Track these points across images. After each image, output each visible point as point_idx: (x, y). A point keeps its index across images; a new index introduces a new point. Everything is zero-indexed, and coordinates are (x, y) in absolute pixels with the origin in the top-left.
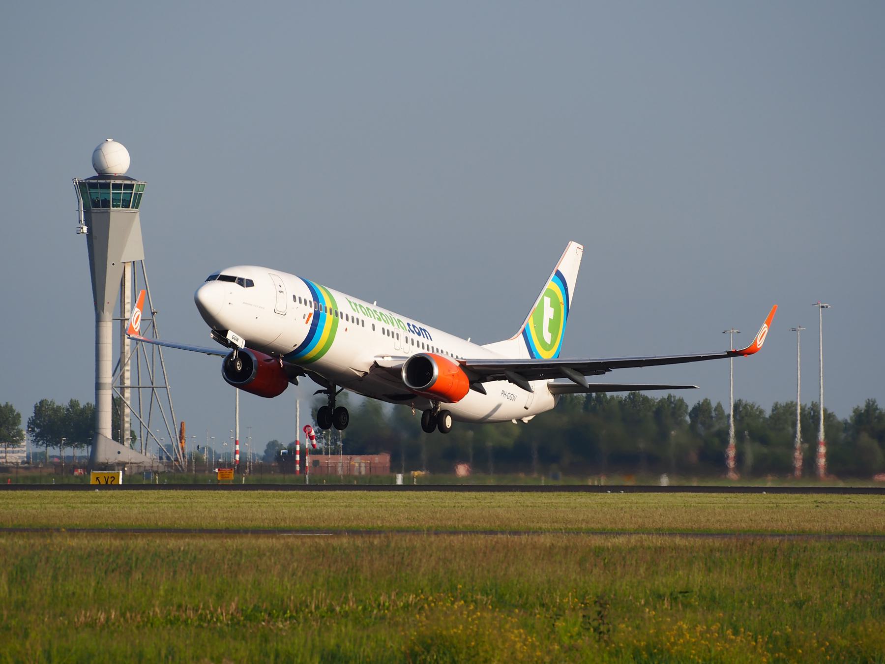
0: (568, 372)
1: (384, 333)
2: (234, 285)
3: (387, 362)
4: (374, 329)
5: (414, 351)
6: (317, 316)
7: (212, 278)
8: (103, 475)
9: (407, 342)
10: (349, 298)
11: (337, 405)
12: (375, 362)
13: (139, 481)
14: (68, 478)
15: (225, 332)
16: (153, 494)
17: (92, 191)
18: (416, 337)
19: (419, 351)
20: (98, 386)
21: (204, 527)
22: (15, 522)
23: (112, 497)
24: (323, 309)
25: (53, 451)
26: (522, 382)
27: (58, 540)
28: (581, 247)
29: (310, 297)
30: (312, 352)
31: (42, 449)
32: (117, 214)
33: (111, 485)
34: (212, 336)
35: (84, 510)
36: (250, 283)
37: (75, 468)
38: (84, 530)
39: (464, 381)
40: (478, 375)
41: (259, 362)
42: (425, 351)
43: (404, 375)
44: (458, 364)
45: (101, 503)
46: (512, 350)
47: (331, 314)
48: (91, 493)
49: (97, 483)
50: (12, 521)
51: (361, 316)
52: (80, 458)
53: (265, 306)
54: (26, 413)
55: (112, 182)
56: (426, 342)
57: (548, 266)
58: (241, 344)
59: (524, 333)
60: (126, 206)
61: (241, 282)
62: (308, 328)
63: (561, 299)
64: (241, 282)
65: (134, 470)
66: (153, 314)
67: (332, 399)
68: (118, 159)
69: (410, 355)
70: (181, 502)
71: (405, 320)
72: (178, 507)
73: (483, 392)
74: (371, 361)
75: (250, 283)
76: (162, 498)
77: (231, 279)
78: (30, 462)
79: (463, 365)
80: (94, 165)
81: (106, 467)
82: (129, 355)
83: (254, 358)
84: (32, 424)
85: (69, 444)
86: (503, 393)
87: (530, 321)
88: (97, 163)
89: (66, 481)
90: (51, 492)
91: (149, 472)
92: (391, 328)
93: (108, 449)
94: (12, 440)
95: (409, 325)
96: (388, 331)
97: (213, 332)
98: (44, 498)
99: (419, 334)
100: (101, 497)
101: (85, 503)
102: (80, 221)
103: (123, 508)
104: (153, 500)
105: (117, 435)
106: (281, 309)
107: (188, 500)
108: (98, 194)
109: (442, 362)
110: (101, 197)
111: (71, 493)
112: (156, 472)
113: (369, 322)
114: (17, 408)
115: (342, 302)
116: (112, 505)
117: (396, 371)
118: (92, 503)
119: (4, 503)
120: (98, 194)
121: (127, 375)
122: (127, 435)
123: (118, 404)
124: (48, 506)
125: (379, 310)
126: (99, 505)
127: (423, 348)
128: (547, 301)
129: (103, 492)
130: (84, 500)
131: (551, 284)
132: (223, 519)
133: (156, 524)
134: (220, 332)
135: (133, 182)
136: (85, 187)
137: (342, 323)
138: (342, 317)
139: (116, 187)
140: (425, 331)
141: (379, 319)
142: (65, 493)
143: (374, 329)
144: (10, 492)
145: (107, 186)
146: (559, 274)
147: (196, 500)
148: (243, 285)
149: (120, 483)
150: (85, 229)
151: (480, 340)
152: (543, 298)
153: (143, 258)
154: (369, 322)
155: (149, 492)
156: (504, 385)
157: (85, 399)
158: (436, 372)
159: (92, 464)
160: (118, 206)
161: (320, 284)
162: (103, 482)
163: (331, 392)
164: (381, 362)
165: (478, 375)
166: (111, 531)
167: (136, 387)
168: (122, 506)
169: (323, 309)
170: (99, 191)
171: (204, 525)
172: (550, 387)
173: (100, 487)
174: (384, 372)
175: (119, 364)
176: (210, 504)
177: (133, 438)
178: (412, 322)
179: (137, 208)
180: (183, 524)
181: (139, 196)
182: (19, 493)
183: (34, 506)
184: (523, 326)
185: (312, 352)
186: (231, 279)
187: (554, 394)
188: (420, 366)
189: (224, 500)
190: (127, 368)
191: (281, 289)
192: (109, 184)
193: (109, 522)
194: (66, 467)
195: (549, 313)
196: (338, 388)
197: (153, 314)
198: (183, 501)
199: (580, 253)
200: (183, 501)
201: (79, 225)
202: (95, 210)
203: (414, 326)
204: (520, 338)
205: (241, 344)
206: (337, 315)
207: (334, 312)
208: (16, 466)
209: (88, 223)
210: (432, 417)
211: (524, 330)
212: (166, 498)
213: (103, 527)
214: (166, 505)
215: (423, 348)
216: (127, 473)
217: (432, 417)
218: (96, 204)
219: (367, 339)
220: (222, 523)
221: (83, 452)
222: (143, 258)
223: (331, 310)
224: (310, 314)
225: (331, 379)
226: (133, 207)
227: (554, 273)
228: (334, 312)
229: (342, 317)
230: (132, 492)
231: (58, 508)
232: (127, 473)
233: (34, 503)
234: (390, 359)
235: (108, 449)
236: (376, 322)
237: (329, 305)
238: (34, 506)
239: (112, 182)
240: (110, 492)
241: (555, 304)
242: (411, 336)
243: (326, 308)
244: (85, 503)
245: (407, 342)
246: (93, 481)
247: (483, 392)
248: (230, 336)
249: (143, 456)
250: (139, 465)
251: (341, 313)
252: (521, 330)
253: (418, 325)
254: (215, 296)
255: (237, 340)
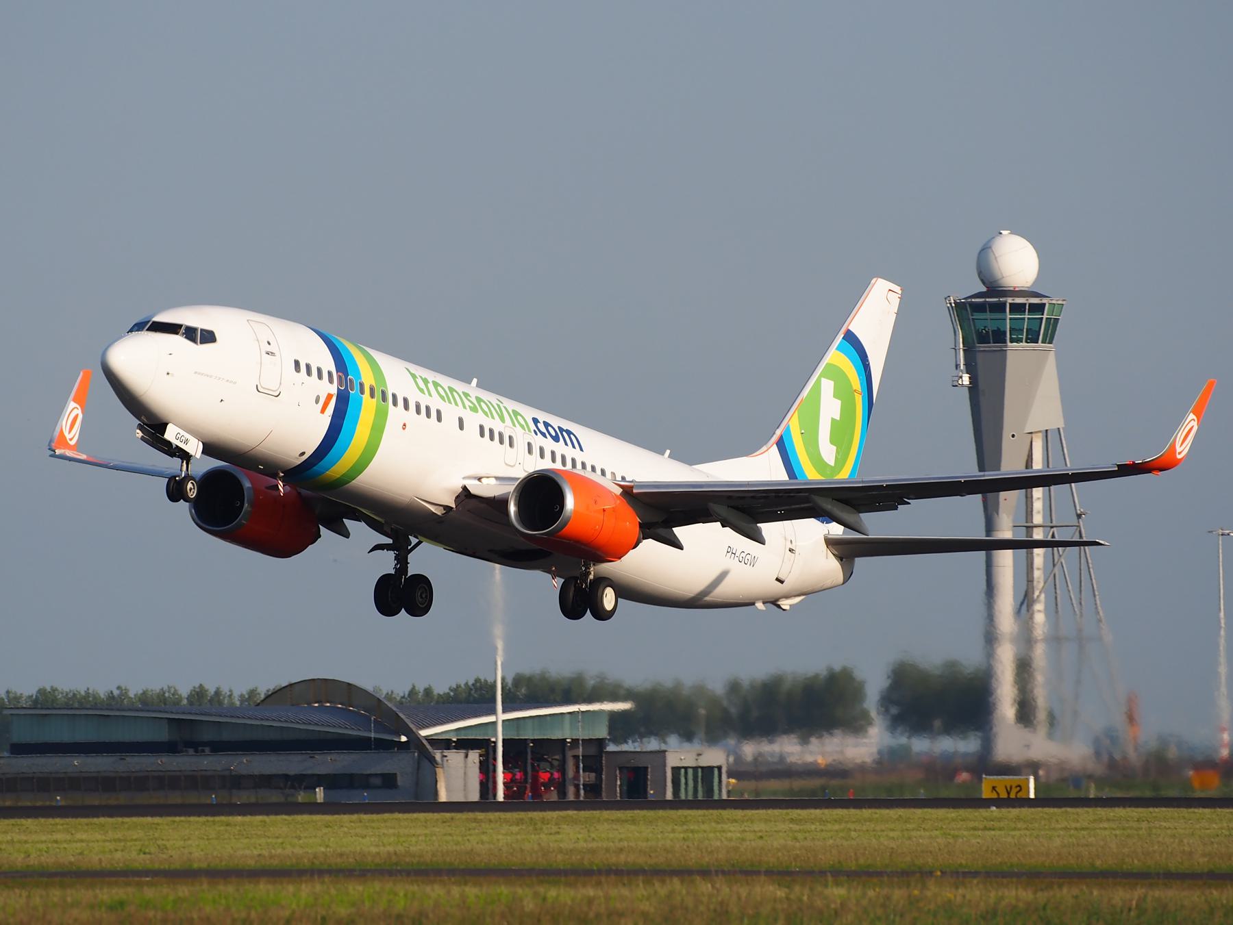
0: (828, 505)
1: (482, 435)
2: (178, 340)
3: (488, 488)
4: (461, 427)
5: (526, 465)
6: (343, 401)
7: (139, 327)
8: (1002, 781)
9: (530, 451)
10: (415, 369)
11: (412, 571)
12: (465, 488)
13: (1062, 793)
14: (946, 789)
15: (163, 427)
16: (1085, 815)
17: (977, 316)
18: (549, 444)
19: (546, 464)
20: (991, 638)
21: (1173, 869)
22: (862, 861)
23: (1018, 819)
24: (357, 387)
25: (921, 745)
26: (743, 524)
27: (932, 889)
28: (897, 289)
29: (329, 364)
30: (339, 466)
31: (903, 740)
32: (1018, 354)
33: (1017, 799)
34: (139, 434)
35: (973, 841)
36: (208, 337)
37: (955, 771)
38: (975, 874)
39: (630, 521)
40: (664, 512)
41: (255, 489)
42: (558, 465)
43: (512, 508)
44: (619, 491)
45: (1000, 829)
46: (761, 469)
47: (372, 396)
48: (983, 812)
49: (994, 796)
50: (857, 860)
51: (435, 403)
52: (966, 755)
53: (244, 381)
54: (875, 683)
55: (1010, 300)
56: (570, 453)
57: (830, 320)
58: (194, 447)
59: (781, 445)
60: (1035, 340)
61: (190, 333)
62: (325, 421)
63: (856, 382)
64: (190, 333)
65: (1054, 776)
66: (1079, 516)
67: (402, 562)
68: (1018, 263)
69: (522, 474)
70: (1131, 828)
71: (528, 413)
72: (1128, 836)
73: (677, 545)
74: (456, 484)
75: (208, 337)
76: (1101, 820)
77: (172, 329)
78: (890, 760)
79: (628, 492)
80: (980, 274)
81: (1006, 769)
82: (1042, 584)
83: (247, 484)
84: (887, 700)
85: (948, 730)
86: (730, 551)
87: (793, 424)
88: (985, 272)
89: (945, 793)
90: (919, 812)
91: (1076, 779)
92: (498, 427)
93: (1010, 741)
94: (855, 724)
95: (535, 421)
96: (491, 431)
97: (140, 427)
98: (907, 821)
99: (556, 439)
100: (1000, 819)
101: (975, 829)
102: (957, 366)
103: (1037, 837)
104: (1085, 824)
105: (1025, 713)
106: (270, 384)
107: (1144, 825)
108: (986, 321)
109: (584, 486)
110: (991, 326)
111: (951, 813)
112: (1090, 777)
113: (452, 414)
114: (859, 674)
115: (397, 375)
116: (1017, 833)
117: (499, 504)
118: (985, 829)
119: (843, 830)
120: (986, 321)
121: (1040, 618)
122: (1041, 715)
123: (1024, 667)
124: (914, 833)
125: (487, 396)
126: (998, 833)
127: (554, 460)
128: (827, 386)
129: (1004, 810)
130: (972, 824)
131: (837, 357)
132: (1204, 855)
133: (1093, 865)
134: (154, 428)
135: (1044, 301)
136: (964, 311)
137: (396, 414)
138: (395, 403)
139: (1017, 308)
140: (569, 433)
141: (474, 409)
142: (941, 812)
143: (461, 427)
144: (853, 811)
145: (1000, 308)
146: (851, 338)
147: (1157, 824)
148: (193, 340)
149: (1032, 796)
150: (966, 379)
151: (689, 458)
152: (819, 380)
153: (1061, 425)
154: (452, 414)
155: (1079, 810)
156: (713, 530)
157: (969, 657)
158: (570, 503)
159: (984, 765)
160: (1019, 341)
161: (356, 342)
162: (1004, 795)
163: (402, 550)
164: (476, 488)
165: (664, 512)
166: (1018, 875)
167: (1055, 639)
168: (1035, 833)
169: (357, 387)
170: (988, 315)
171: (1173, 866)
172: (831, 543)
173: (999, 803)
174: (483, 505)
175: (1025, 602)
176: (1182, 831)
177: (1052, 719)
178: (543, 417)
179: (1050, 343)
180: (1136, 864)
181: (1053, 324)
182: (866, 813)
183: (892, 834)
184: (778, 432)
185: (339, 466)
186: (172, 329)
187: (840, 558)
188: (541, 492)
189: (1204, 824)
190: (1039, 607)
191: (269, 348)
192: (1004, 304)
193: (1015, 860)
194: (941, 770)
195: (830, 408)
196: (414, 541)
197: (1079, 516)
198: (1135, 825)
199: (895, 300)
200: (1135, 825)
201: (955, 373)
202: (982, 347)
203: (546, 425)
204: (774, 450)
205: (194, 447)
206: (384, 399)
207: (378, 394)
208: (862, 768)
209: (970, 368)
210: (578, 590)
211: (781, 438)
212: (1108, 820)
213: (1005, 868)
214: (1107, 833)
215: (554, 460)
216: (1043, 780)
217: (578, 590)
218: (983, 338)
219: (443, 441)
220: (1201, 862)
221: (964, 745)
222: (1061, 425)
223: (372, 390)
224: (330, 396)
225: (400, 523)
226: (1043, 342)
227: (841, 336)
228: (378, 394)
229: (395, 403)
230: (1052, 810)
231: (930, 837)
232: (1043, 780)
233: (892, 830)
234: (493, 481)
235: (1010, 741)
236: (468, 416)
237: (368, 379)
238: (892, 834)
239: (1010, 300)
240: (1015, 812)
241: (843, 392)
242: (539, 441)
243: (362, 385)
244: (975, 829)
245: (530, 451)
246: (986, 793)
247: (677, 545)
248: (171, 434)
249: (1067, 750)
250: (1061, 766)
251: (394, 396)
252: (775, 438)
253: (556, 422)
254: (143, 361)
255: (186, 442)
